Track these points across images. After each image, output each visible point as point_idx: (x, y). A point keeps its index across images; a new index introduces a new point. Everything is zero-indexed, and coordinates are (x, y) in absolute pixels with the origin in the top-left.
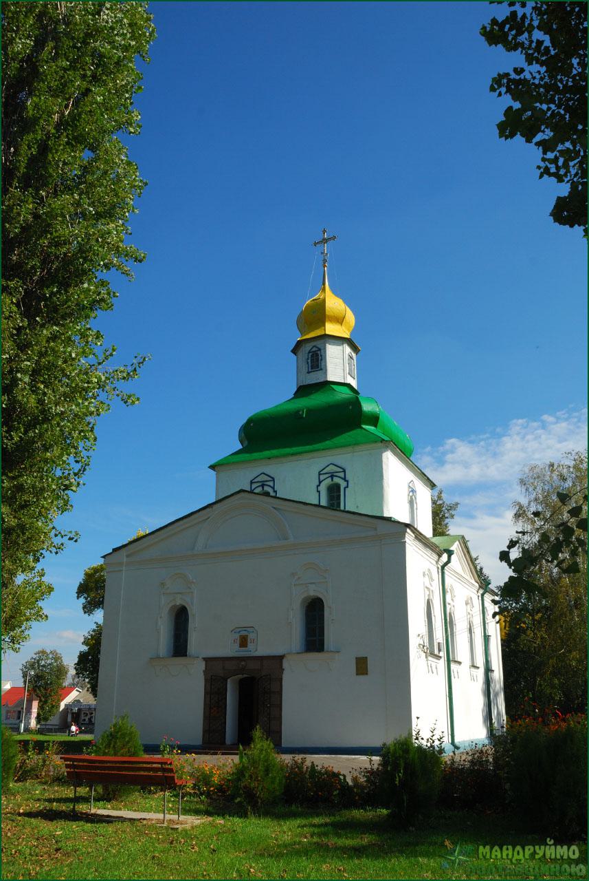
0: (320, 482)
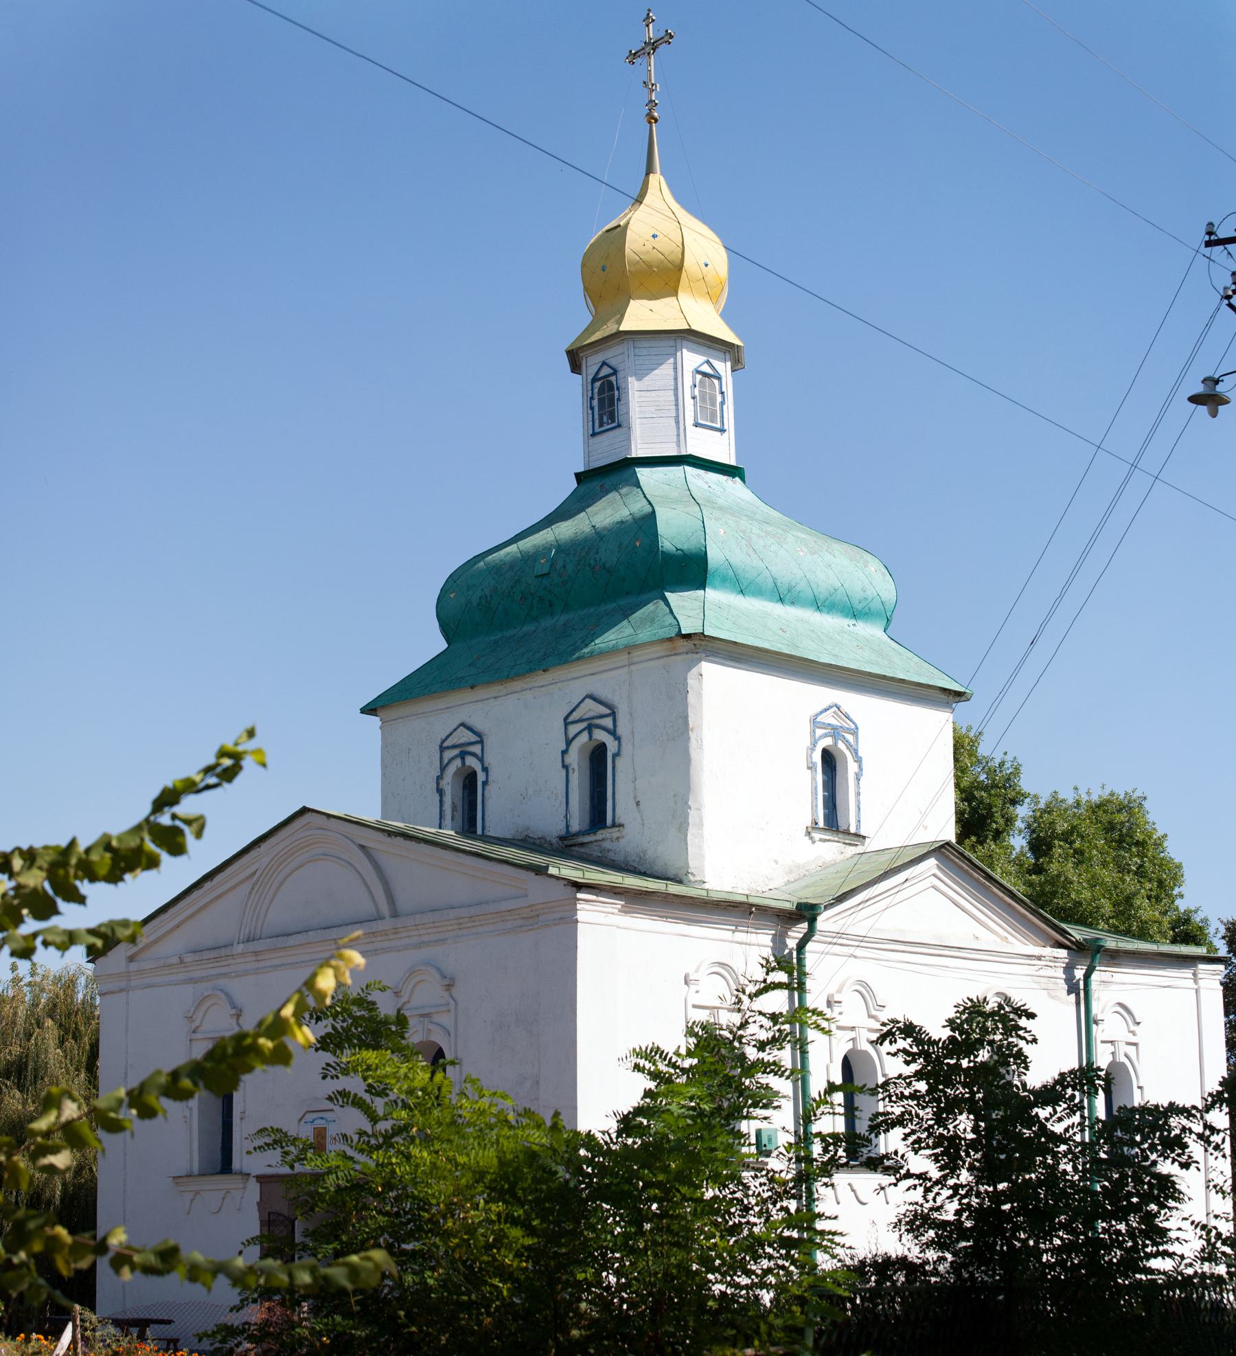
0: (569, 742)
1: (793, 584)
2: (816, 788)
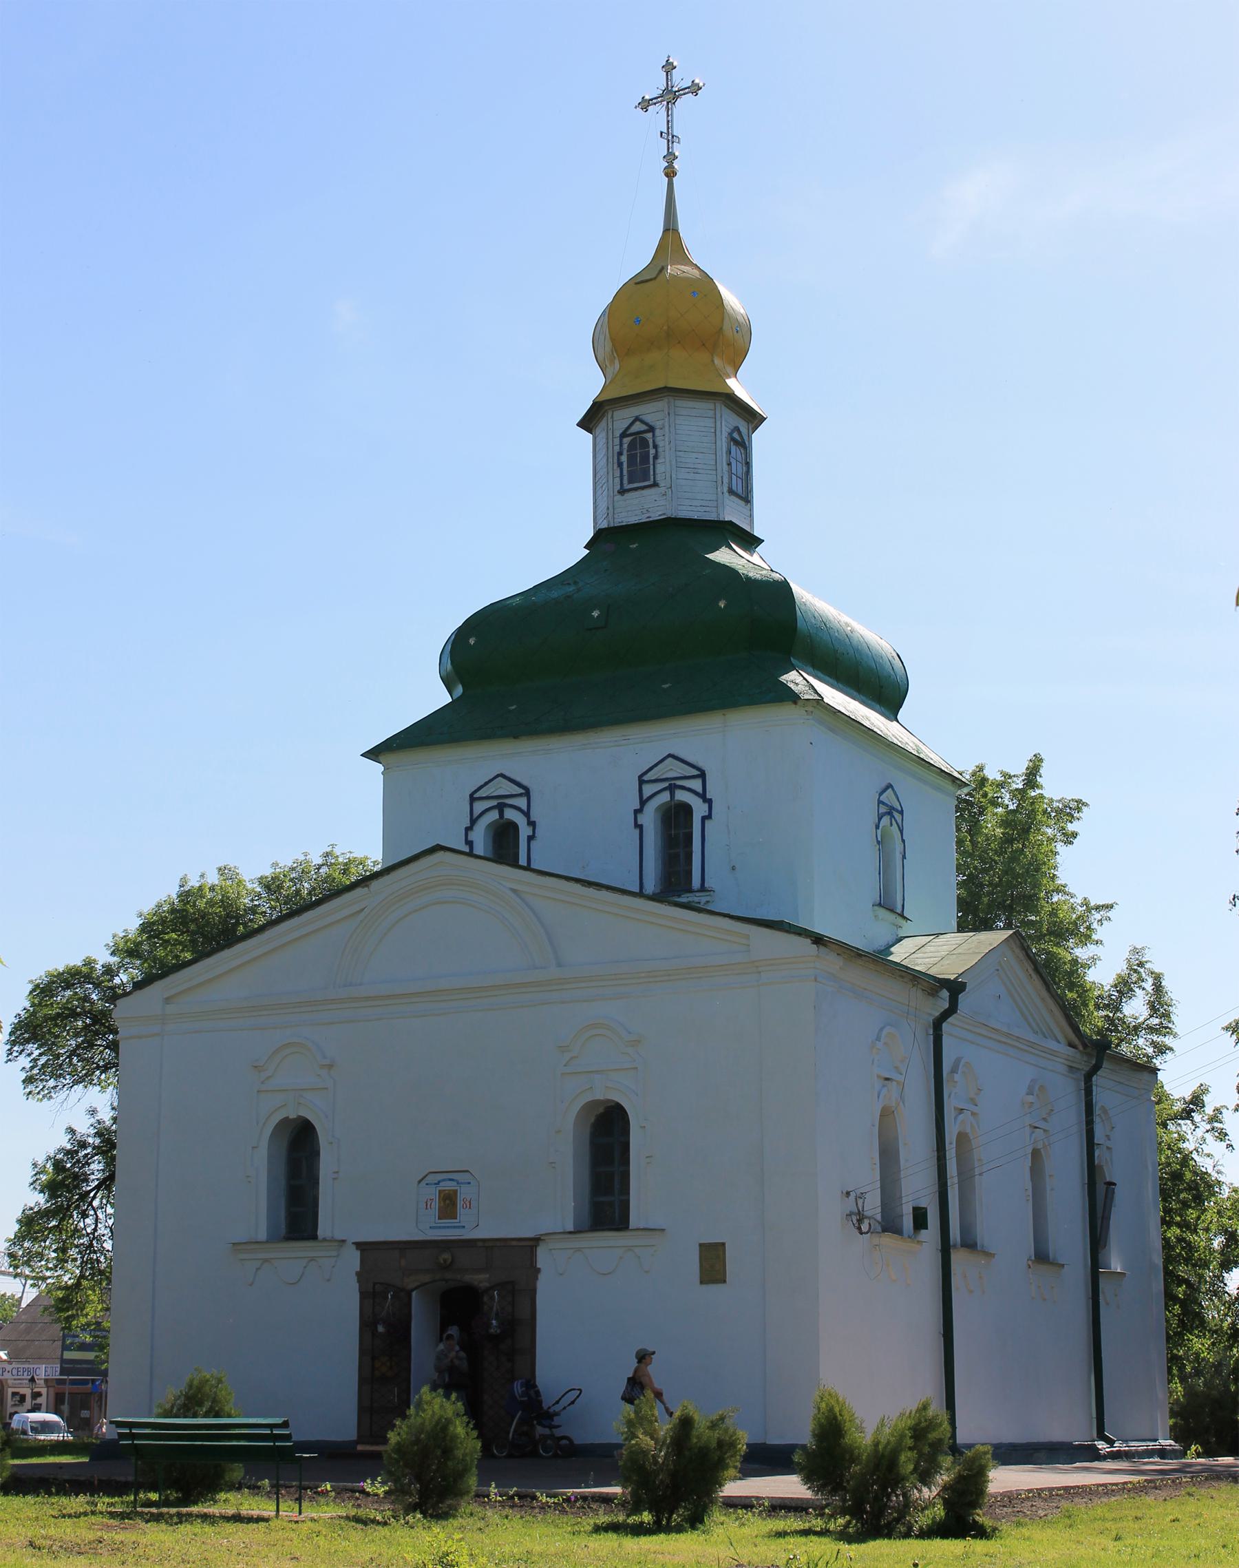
0: (643, 802)
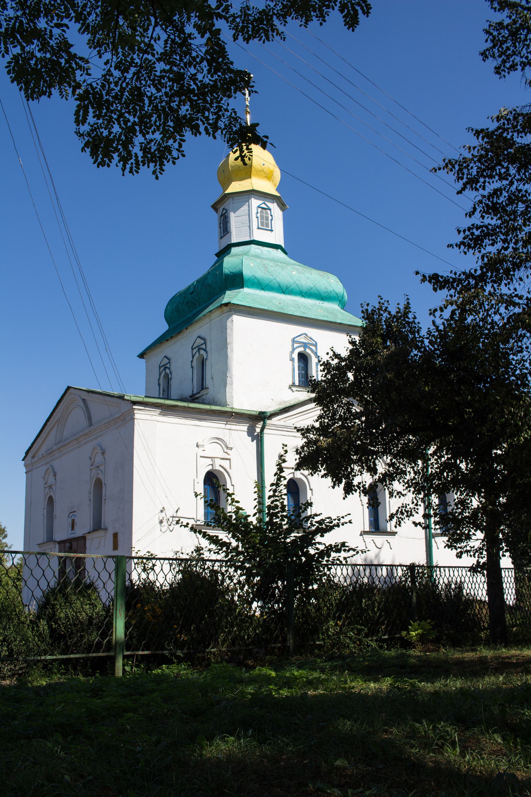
1: (289, 285)
2: (294, 368)
